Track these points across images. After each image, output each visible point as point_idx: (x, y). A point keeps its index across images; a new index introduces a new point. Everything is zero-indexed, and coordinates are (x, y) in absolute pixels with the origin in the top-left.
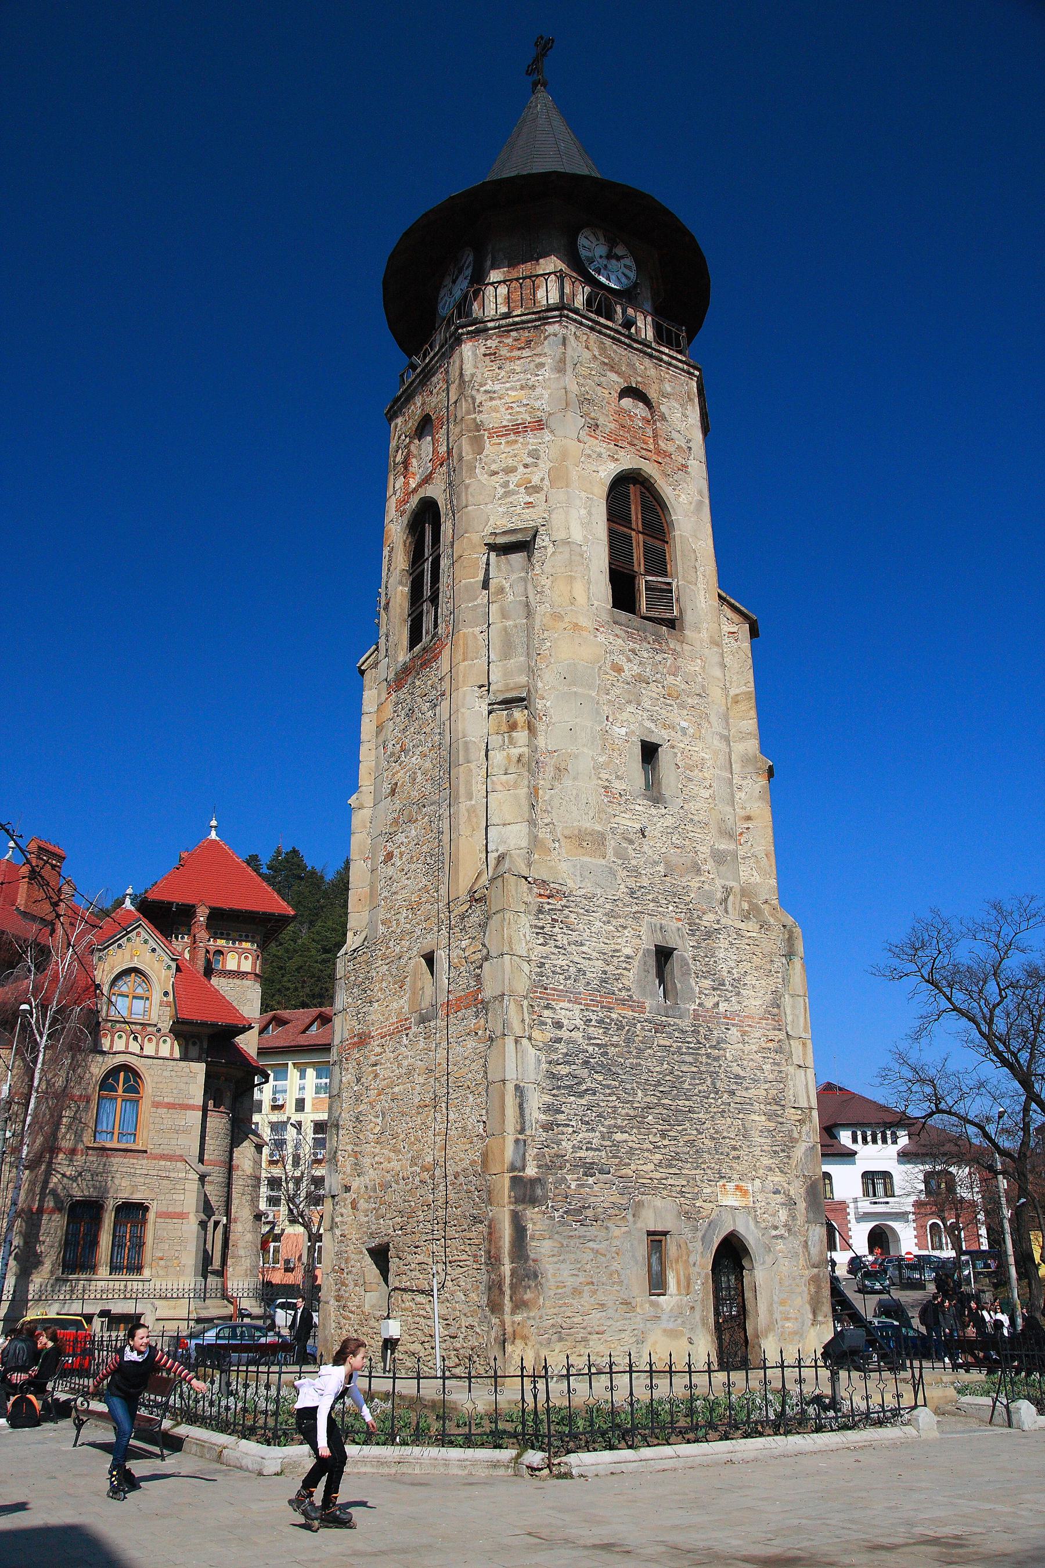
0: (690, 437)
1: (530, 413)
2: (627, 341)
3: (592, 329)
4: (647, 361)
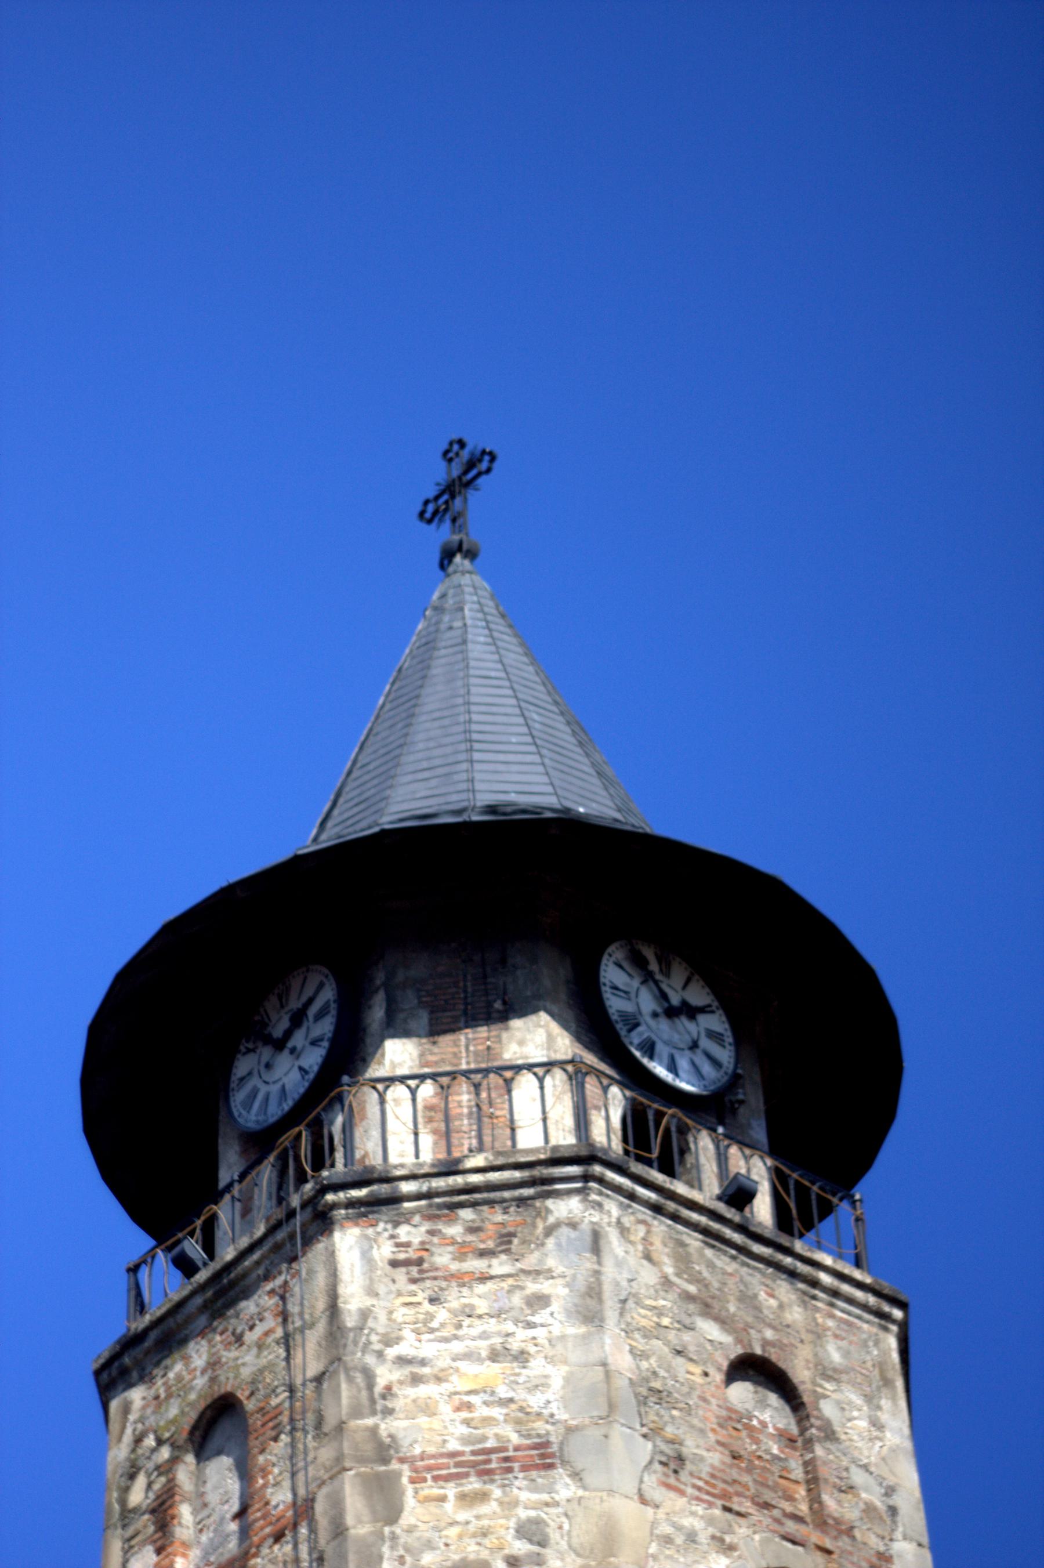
0: (891, 1480)
1: (518, 1422)
2: (737, 1238)
3: (657, 1209)
4: (784, 1289)
